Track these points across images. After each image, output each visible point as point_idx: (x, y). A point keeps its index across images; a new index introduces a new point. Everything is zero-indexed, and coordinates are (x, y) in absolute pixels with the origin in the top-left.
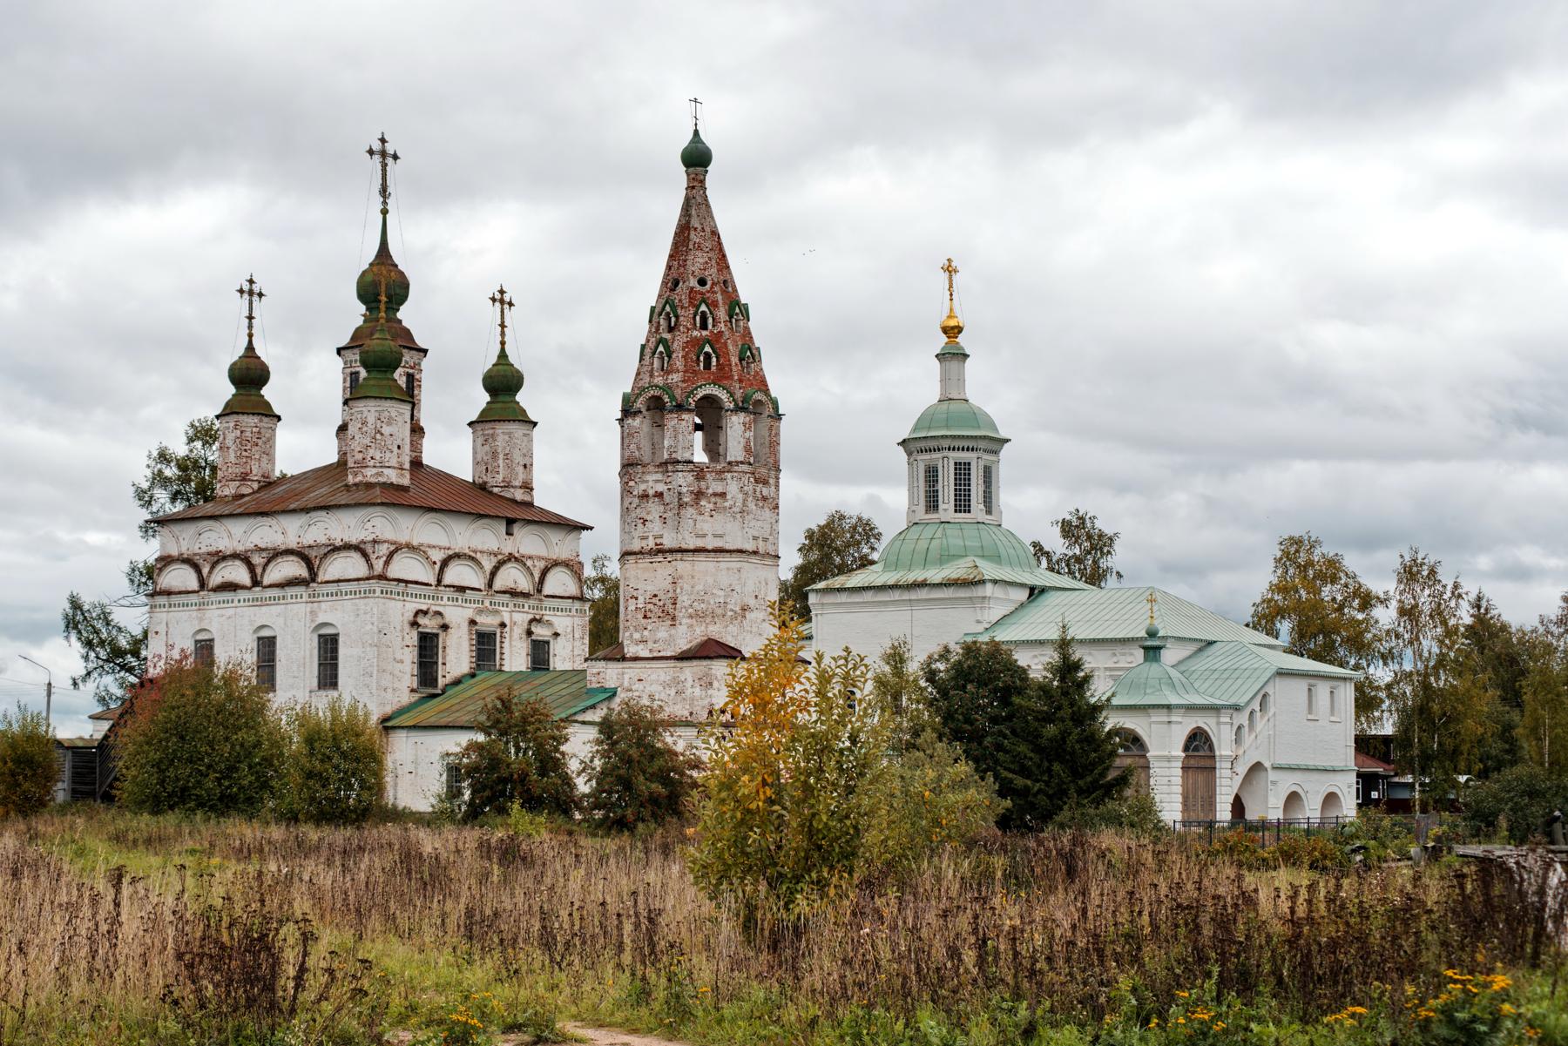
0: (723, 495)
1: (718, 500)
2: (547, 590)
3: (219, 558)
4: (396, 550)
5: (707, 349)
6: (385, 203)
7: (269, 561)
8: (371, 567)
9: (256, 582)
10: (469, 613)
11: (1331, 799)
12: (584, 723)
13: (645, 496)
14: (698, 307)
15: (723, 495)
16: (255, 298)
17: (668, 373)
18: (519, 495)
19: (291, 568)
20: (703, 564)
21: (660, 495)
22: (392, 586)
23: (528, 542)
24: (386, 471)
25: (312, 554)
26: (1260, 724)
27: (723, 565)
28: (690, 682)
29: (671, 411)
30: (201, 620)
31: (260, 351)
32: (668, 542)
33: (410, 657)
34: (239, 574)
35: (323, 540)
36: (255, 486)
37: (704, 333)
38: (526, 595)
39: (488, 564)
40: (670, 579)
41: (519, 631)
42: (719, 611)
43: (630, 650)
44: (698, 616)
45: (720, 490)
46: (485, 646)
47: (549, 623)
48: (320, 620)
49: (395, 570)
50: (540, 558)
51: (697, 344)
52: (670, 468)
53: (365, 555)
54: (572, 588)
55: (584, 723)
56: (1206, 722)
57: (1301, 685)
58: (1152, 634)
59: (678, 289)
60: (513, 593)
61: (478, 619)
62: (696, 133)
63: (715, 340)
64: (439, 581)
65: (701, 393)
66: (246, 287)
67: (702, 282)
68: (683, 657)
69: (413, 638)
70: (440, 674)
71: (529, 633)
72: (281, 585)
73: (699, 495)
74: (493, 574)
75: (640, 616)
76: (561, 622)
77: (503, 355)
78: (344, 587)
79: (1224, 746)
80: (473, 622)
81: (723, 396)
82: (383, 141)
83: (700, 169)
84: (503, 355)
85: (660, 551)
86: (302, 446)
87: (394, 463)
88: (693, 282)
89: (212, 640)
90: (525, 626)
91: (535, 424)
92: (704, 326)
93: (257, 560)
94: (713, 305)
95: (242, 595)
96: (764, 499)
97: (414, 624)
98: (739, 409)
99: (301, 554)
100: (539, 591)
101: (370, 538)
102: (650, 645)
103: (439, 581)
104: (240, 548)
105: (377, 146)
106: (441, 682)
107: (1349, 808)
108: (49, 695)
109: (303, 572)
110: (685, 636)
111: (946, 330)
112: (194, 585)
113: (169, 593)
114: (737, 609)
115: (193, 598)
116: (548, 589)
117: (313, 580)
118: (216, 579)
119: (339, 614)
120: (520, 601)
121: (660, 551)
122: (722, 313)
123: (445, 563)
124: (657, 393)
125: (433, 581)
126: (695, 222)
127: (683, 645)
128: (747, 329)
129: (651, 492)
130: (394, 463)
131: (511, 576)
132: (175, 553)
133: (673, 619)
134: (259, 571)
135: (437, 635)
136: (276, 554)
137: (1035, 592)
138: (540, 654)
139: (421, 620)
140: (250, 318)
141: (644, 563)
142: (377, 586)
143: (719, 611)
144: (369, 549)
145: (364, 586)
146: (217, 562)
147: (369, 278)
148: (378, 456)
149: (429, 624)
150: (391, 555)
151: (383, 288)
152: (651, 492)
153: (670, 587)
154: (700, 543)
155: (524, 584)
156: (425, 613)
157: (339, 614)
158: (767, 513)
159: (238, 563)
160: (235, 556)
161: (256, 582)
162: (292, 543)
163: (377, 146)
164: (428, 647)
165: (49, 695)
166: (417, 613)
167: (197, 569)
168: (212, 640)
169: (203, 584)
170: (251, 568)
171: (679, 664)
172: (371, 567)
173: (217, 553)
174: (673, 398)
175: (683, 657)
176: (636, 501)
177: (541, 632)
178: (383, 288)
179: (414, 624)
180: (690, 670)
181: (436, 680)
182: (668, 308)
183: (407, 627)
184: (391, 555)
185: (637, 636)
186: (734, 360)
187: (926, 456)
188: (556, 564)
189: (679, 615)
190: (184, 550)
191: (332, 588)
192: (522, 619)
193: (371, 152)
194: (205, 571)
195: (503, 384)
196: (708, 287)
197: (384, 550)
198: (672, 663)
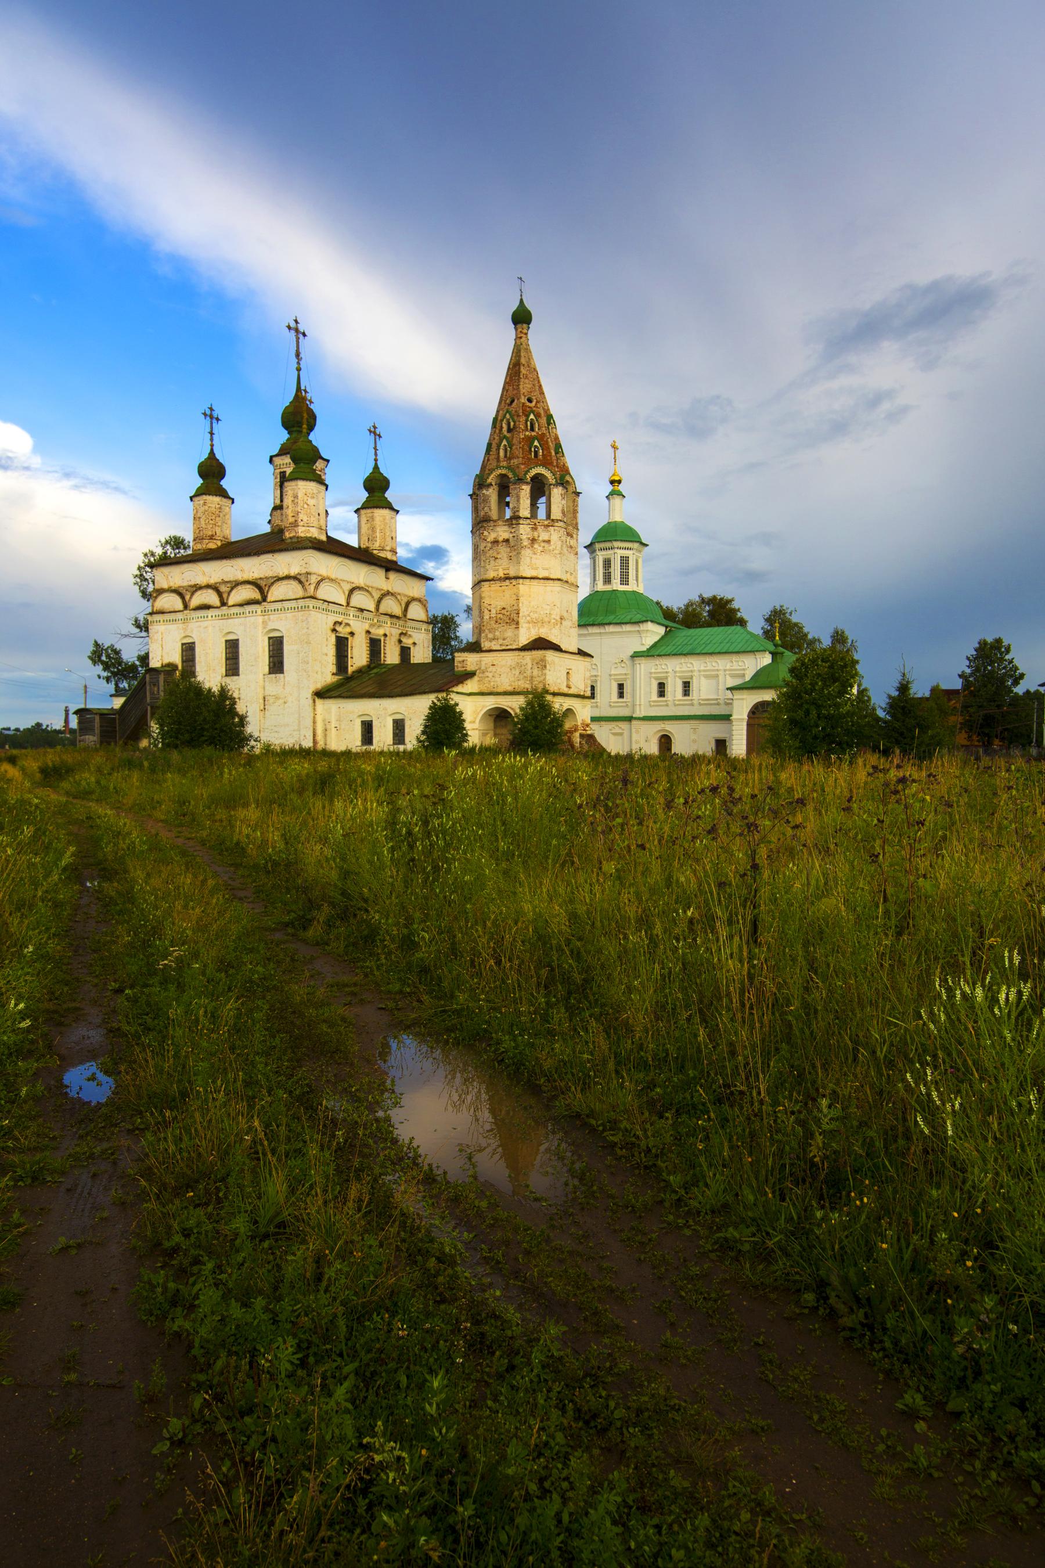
0: (549, 542)
1: (546, 545)
2: (409, 616)
3: (197, 588)
4: (322, 580)
5: (536, 443)
6: (298, 363)
7: (232, 589)
8: (305, 590)
9: (223, 604)
10: (367, 627)
12: (458, 693)
13: (496, 542)
14: (528, 416)
15: (549, 542)
16: (214, 421)
17: (510, 459)
18: (389, 556)
19: (253, 593)
20: (536, 587)
21: (507, 541)
22: (319, 604)
24: (312, 529)
25: (262, 583)
27: (549, 589)
28: (530, 665)
29: (515, 483)
30: (185, 629)
31: (218, 456)
32: (512, 574)
33: (331, 651)
34: (212, 598)
35: (270, 574)
36: (219, 543)
37: (533, 434)
38: (398, 618)
39: (377, 596)
40: (515, 597)
42: (546, 619)
44: (534, 622)
45: (546, 538)
46: (375, 646)
47: (410, 636)
48: (270, 627)
49: (321, 593)
50: (405, 596)
51: (530, 440)
52: (514, 522)
53: (300, 582)
54: (423, 616)
55: (458, 693)
59: (514, 404)
61: (372, 631)
62: (521, 301)
63: (541, 438)
64: (348, 604)
65: (534, 472)
66: (208, 412)
67: (530, 400)
68: (524, 649)
69: (333, 639)
70: (350, 664)
71: (400, 641)
72: (241, 605)
73: (533, 540)
74: (379, 602)
75: (493, 622)
77: (212, 452)
78: (287, 604)
80: (368, 632)
81: (548, 474)
82: (296, 321)
83: (525, 326)
84: (212, 452)
85: (507, 578)
86: (249, 511)
87: (315, 524)
88: (523, 400)
89: (194, 643)
90: (397, 637)
91: (398, 512)
92: (532, 429)
93: (223, 589)
94: (538, 416)
95: (210, 613)
96: (571, 547)
97: (334, 630)
98: (557, 485)
99: (254, 583)
100: (405, 616)
101: (304, 571)
102: (501, 641)
103: (348, 604)
104: (212, 581)
105: (293, 325)
106: (350, 670)
108: (86, 692)
109: (257, 596)
110: (525, 636)
111: (612, 482)
112: (181, 607)
113: (162, 612)
114: (558, 618)
115: (179, 616)
117: (264, 599)
118: (197, 600)
119: (283, 623)
120: (395, 620)
121: (507, 578)
122: (543, 420)
123: (352, 591)
124: (504, 472)
125: (344, 604)
126: (523, 361)
127: (524, 641)
128: (557, 438)
129: (501, 539)
130: (315, 524)
131: (391, 606)
132: (166, 586)
133: (518, 623)
134: (225, 596)
135: (347, 639)
136: (236, 584)
138: (405, 652)
139: (338, 628)
140: (212, 434)
142: (311, 603)
143: (546, 619)
144: (303, 579)
145: (301, 603)
146: (196, 591)
147: (291, 410)
148: (305, 519)
149: (343, 631)
150: (318, 583)
152: (501, 539)
153: (514, 602)
154: (534, 574)
155: (397, 611)
156: (340, 623)
157: (283, 623)
158: (572, 556)
159: (210, 591)
161: (223, 604)
162: (247, 576)
164: (342, 646)
165: (86, 692)
166: (335, 623)
168: (194, 643)
169: (186, 606)
170: (220, 594)
171: (522, 653)
172: (305, 590)
173: (195, 585)
174: (514, 474)
175: (524, 649)
176: (489, 545)
177: (407, 642)
179: (334, 630)
180: (528, 657)
181: (347, 668)
182: (508, 416)
183: (329, 632)
184: (318, 583)
185: (490, 636)
186: (553, 453)
187: (604, 553)
188: (414, 599)
189: (522, 621)
190: (172, 584)
191: (278, 605)
192: (395, 632)
193: (289, 328)
194: (187, 597)
196: (533, 404)
197: (314, 579)
198: (517, 653)
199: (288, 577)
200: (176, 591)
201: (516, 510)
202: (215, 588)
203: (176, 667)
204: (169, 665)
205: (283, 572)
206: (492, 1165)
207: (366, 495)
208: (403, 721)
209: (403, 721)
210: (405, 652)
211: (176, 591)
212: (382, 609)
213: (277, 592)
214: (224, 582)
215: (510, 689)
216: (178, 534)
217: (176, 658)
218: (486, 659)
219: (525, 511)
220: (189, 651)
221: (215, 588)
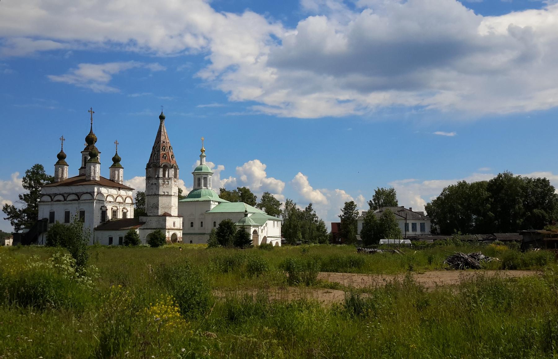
3: (56, 195)
9: (65, 200)
11: (277, 243)
13: (152, 184)
19: (74, 197)
23: (122, 192)
26: (266, 228)
31: (64, 151)
34: (61, 198)
41: (121, 210)
43: (149, 214)
46: (115, 213)
56: (257, 229)
57: (272, 222)
58: (246, 211)
60: (110, 202)
69: (101, 212)
73: (163, 184)
76: (129, 209)
77: (62, 151)
79: (260, 233)
84: (62, 151)
93: (65, 195)
97: (101, 209)
99: (76, 194)
104: (61, 193)
107: (280, 245)
115: (49, 203)
116: (126, 202)
117: (79, 199)
118: (57, 198)
131: (119, 199)
136: (69, 194)
137: (219, 203)
138: (125, 214)
141: (152, 197)
151: (90, 140)
155: (122, 201)
160: (60, 194)
161: (65, 200)
162: (74, 192)
163: (90, 110)
167: (51, 197)
169: (52, 200)
170: (64, 197)
178: (90, 140)
191: (84, 201)
192: (121, 208)
195: (116, 160)
199: (87, 193)
200: (49, 195)
201: (158, 175)
202: (62, 195)
203: (48, 220)
204: (46, 219)
205: (85, 191)
206: (77, 72)
207: (113, 163)
208: (69, 212)
209: (69, 212)
210: (125, 214)
211: (49, 195)
212: (117, 201)
213: (84, 197)
214: (65, 193)
215: (155, 227)
216: (36, 163)
217: (47, 216)
218: (148, 219)
219: (161, 175)
220: (52, 214)
221: (62, 195)
